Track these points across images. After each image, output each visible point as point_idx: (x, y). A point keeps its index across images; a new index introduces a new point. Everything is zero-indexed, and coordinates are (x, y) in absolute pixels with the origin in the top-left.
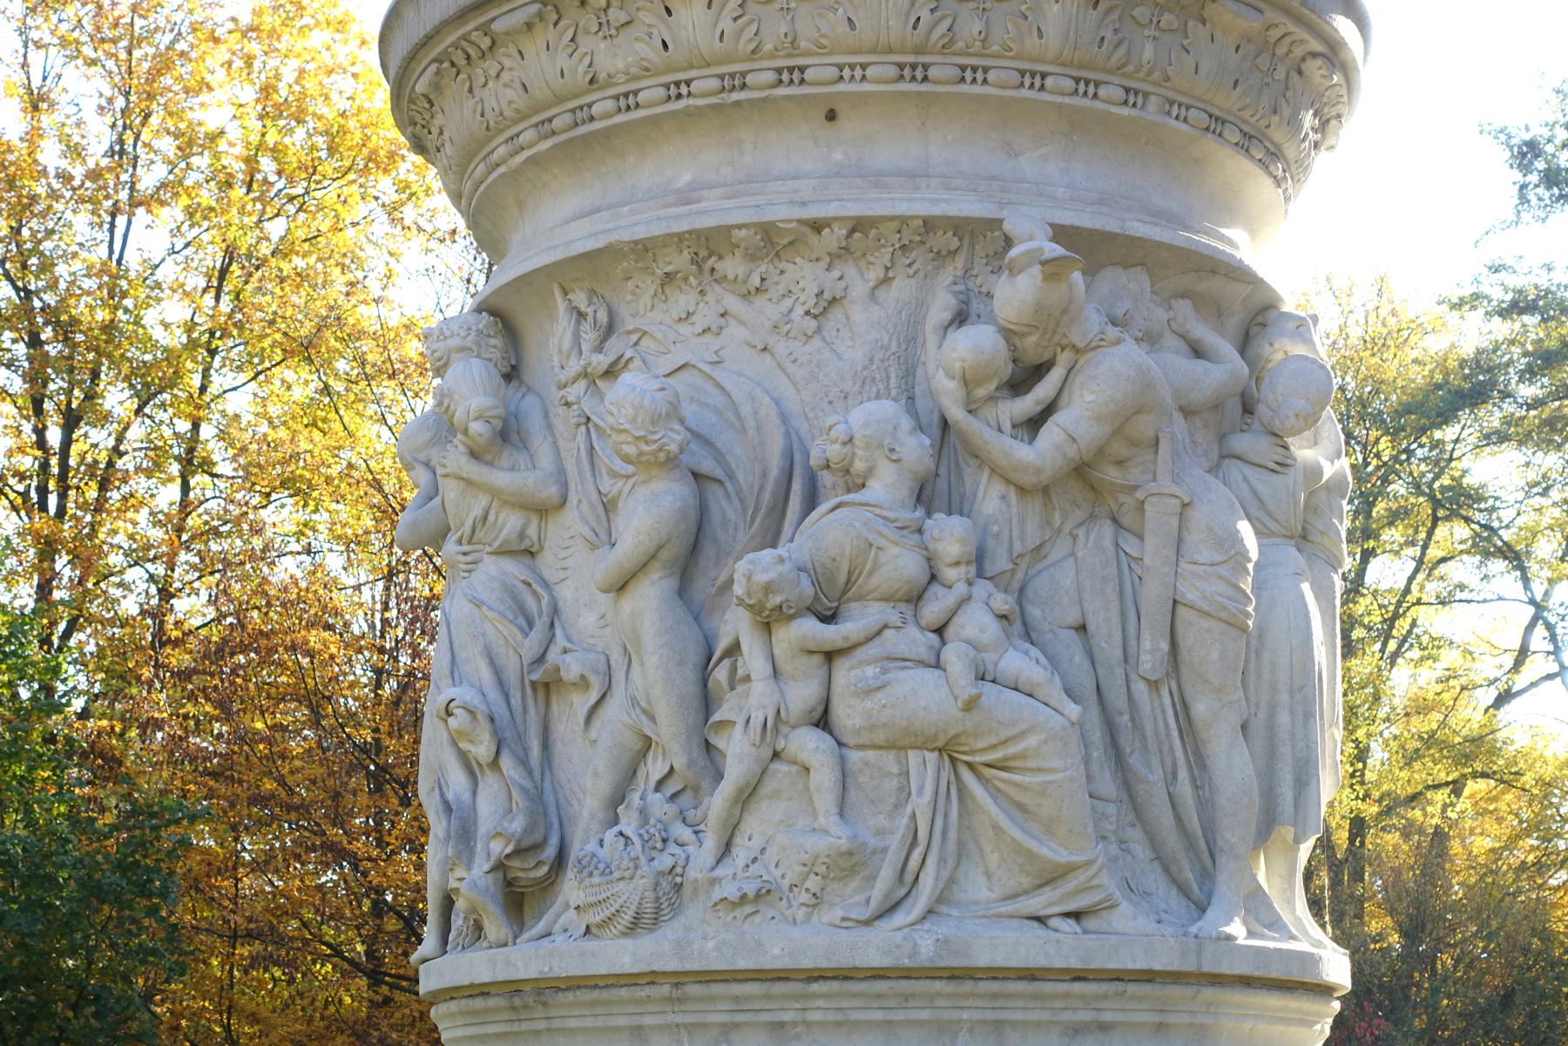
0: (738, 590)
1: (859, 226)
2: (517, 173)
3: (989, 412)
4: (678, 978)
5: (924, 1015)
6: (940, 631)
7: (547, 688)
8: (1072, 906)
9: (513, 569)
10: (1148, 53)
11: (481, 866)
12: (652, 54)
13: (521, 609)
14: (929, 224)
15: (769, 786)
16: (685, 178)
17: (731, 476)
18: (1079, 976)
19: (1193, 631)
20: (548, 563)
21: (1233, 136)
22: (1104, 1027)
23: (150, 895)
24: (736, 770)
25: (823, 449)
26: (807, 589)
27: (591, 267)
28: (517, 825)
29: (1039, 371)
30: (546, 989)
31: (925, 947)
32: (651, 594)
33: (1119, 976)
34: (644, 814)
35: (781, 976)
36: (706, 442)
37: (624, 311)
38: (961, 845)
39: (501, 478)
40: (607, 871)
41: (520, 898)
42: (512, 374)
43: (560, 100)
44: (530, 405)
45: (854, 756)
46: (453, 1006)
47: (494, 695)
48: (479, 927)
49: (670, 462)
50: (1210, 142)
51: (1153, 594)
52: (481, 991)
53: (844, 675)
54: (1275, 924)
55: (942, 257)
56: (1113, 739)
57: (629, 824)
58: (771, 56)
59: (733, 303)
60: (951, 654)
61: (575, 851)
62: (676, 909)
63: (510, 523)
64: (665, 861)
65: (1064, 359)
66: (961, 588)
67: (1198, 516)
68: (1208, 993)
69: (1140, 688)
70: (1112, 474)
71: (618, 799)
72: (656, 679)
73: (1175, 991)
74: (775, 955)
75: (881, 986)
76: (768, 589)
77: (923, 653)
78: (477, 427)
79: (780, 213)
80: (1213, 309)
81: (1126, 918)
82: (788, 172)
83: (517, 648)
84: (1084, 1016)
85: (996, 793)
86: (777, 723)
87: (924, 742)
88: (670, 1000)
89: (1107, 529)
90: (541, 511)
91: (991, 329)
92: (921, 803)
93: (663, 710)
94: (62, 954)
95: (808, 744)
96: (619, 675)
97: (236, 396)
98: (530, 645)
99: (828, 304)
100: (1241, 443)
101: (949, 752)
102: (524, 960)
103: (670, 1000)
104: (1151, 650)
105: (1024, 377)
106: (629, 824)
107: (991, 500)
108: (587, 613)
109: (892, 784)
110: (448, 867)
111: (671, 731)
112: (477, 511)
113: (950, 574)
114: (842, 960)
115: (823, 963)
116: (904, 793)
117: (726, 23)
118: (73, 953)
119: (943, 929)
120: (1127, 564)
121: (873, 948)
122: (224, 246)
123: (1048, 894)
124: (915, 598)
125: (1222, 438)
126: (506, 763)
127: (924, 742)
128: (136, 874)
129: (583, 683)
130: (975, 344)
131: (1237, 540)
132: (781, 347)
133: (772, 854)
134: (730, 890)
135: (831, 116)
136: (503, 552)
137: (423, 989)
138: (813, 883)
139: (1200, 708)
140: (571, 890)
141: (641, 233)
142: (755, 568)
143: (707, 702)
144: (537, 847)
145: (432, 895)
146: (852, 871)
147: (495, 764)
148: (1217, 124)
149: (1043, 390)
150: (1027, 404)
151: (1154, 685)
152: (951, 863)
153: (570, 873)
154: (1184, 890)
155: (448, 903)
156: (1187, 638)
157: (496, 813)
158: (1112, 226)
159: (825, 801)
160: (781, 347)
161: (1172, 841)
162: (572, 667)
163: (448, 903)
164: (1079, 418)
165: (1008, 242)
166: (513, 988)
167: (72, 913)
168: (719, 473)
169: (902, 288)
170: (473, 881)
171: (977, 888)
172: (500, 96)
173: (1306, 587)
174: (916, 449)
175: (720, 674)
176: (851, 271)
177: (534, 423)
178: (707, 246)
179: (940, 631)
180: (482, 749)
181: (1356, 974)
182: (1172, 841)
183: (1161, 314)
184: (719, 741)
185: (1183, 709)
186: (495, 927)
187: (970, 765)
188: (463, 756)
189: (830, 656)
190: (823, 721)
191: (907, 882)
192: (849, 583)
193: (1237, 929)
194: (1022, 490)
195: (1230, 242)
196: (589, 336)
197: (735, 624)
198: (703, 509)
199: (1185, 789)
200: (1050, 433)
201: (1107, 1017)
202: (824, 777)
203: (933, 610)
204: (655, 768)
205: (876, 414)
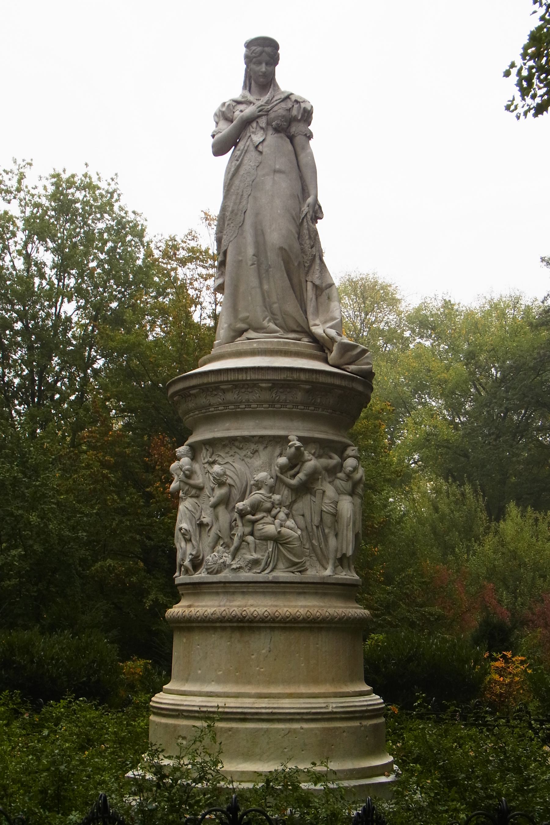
5: (270, 590)
8: (299, 570)
15: (242, 546)
17: (236, 485)
31: (270, 577)
46: (182, 587)
58: (244, 403)
59: (237, 450)
66: (278, 509)
84: (301, 590)
85: (286, 548)
86: (244, 535)
88: (223, 587)
95: (250, 539)
103: (223, 587)
114: (255, 580)
115: (251, 580)
119: (274, 574)
122: (270, 132)
123: (295, 567)
150: (292, 472)
152: (275, 561)
168: (234, 484)
187: (280, 544)
192: (257, 508)
201: (305, 591)
203: (274, 512)
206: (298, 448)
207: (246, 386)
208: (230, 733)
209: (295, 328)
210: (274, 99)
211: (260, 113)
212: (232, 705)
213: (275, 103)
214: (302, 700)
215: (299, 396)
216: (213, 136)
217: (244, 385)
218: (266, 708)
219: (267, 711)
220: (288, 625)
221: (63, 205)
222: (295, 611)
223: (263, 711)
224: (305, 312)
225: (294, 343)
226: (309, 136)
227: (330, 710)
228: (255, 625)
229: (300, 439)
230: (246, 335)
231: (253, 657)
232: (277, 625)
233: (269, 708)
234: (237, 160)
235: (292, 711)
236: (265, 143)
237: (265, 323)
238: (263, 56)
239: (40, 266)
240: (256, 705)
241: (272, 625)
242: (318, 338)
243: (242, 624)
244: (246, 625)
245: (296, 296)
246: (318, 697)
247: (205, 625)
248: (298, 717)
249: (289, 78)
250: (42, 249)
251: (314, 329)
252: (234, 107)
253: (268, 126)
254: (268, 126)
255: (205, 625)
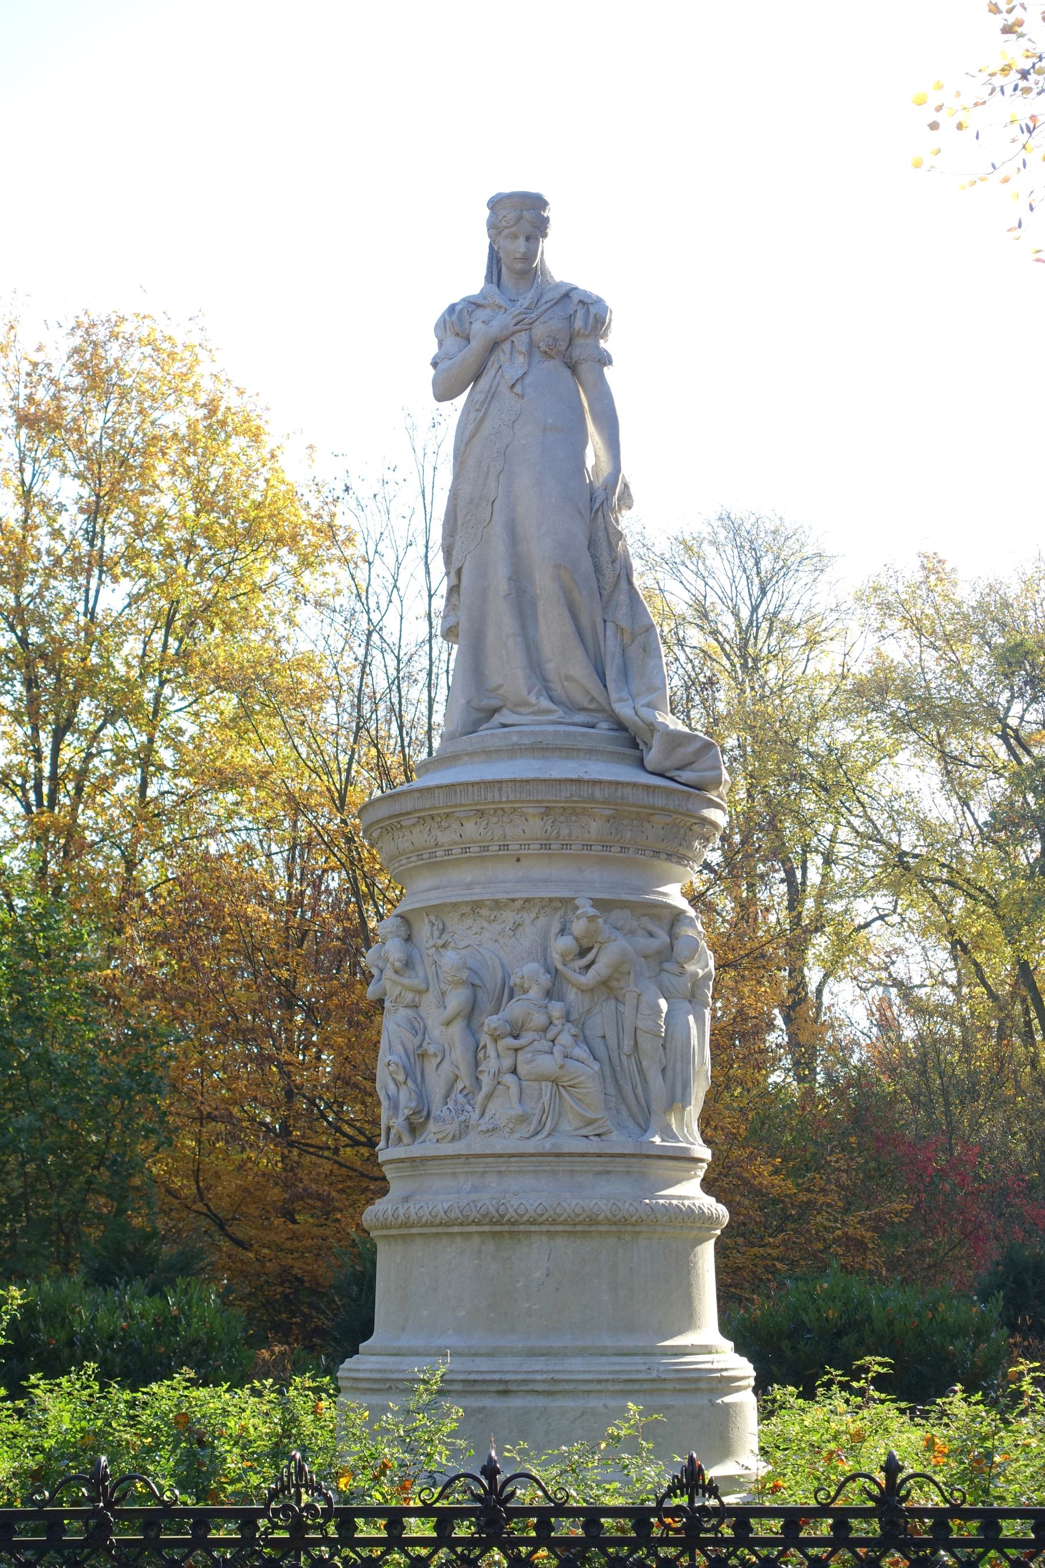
0: (485, 1029)
1: (527, 900)
2: (409, 869)
3: (571, 965)
4: (467, 1156)
6: (553, 1041)
7: (423, 1056)
9: (410, 1013)
10: (628, 835)
11: (401, 1118)
12: (457, 838)
13: (414, 1028)
14: (551, 900)
16: (469, 879)
18: (599, 1155)
19: (642, 1037)
20: (422, 1010)
21: (663, 856)
22: (608, 1172)
23: (150, 1092)
24: (485, 1088)
25: (515, 980)
26: (508, 1028)
27: (437, 909)
28: (413, 1104)
29: (590, 949)
30: (424, 1160)
31: (548, 1146)
32: (458, 1027)
33: (613, 1155)
34: (456, 1102)
35: (501, 1156)
36: (476, 973)
37: (448, 924)
38: (560, 1113)
39: (406, 981)
40: (444, 1121)
41: (414, 1129)
42: (409, 939)
43: (425, 849)
44: (415, 952)
45: (524, 1083)
47: (405, 1058)
48: (400, 1139)
49: (463, 983)
50: (655, 861)
51: (628, 1025)
52: (402, 1161)
53: (521, 1056)
54: (675, 1138)
55: (556, 909)
56: (612, 1074)
57: (451, 1105)
59: (485, 924)
60: (555, 1049)
61: (433, 1114)
62: (467, 1133)
63: (409, 996)
64: (462, 1118)
65: (597, 946)
67: (644, 998)
68: (645, 1161)
69: (624, 1057)
70: (615, 984)
71: (447, 1096)
72: (459, 1055)
73: (633, 1160)
74: (499, 1149)
75: (533, 1159)
76: (495, 1029)
77: (547, 1049)
78: (397, 964)
79: (500, 896)
80: (657, 918)
81: (615, 1136)
82: (503, 879)
83: (413, 1042)
87: (547, 1079)
89: (613, 1002)
90: (420, 992)
91: (570, 938)
92: (546, 1099)
93: (461, 1067)
94: (89, 1132)
95: (509, 1079)
96: (447, 1052)
97: (179, 714)
98: (417, 1041)
99: (517, 926)
100: (667, 966)
101: (555, 1082)
102: (416, 1150)
104: (627, 1044)
105: (583, 952)
106: (451, 1105)
107: (572, 994)
108: (436, 1031)
109: (536, 1093)
110: (389, 1119)
111: (464, 1072)
112: (397, 992)
113: (556, 1022)
114: (521, 1151)
116: (540, 1096)
117: (481, 830)
118: (98, 1132)
120: (619, 1016)
121: (530, 1147)
123: (589, 1128)
124: (545, 1030)
125: (661, 963)
126: (409, 1082)
127: (547, 1079)
128: (140, 1075)
129: (435, 1055)
130: (563, 944)
131: (658, 1006)
132: (501, 941)
133: (497, 1116)
134: (483, 1128)
135: (518, 860)
136: (406, 1007)
137: (380, 1160)
138: (511, 1125)
139: (645, 1064)
140: (432, 1127)
141: (454, 900)
142: (491, 1022)
143: (477, 1064)
144: (420, 1112)
145: (383, 1127)
146: (523, 1121)
147: (405, 1083)
148: (657, 853)
149: (590, 957)
151: (629, 1056)
153: (431, 1121)
154: (639, 1126)
155: (389, 1129)
156: (640, 1040)
157: (406, 1100)
158: (616, 897)
159: (515, 1099)
160: (501, 941)
161: (635, 1109)
162: (431, 1049)
163: (389, 1129)
164: (604, 963)
165: (577, 908)
166: (413, 1160)
167: (98, 1105)
169: (542, 920)
170: (398, 1123)
171: (566, 1126)
172: (404, 844)
173: (691, 1018)
174: (545, 980)
175: (481, 1055)
176: (525, 914)
177: (417, 959)
178: (476, 906)
179: (553, 1041)
180: (401, 1078)
181: (713, 1155)
182: (635, 1109)
183: (635, 924)
184: (480, 1077)
185: (639, 1064)
186: (406, 1139)
188: (394, 1079)
189: (516, 1050)
190: (514, 1071)
191: (541, 1124)
193: (657, 1140)
194: (582, 991)
195: (665, 894)
196: (436, 933)
197: (485, 1039)
198: (475, 997)
199: (639, 1090)
200: (592, 971)
202: (514, 1090)
203: (550, 1035)
204: (460, 1086)
205: (532, 967)
206: (592, 919)
207: (500, 813)
208: (481, 1416)
209: (586, 704)
210: (543, 301)
211: (518, 327)
212: (484, 1368)
213: (544, 308)
214: (604, 1359)
215: (595, 827)
216: (435, 364)
217: (495, 810)
218: (542, 1372)
219: (545, 1376)
220: (579, 1228)
221: (96, 377)
222: (592, 1204)
223: (538, 1377)
224: (602, 677)
225: (583, 734)
226: (605, 360)
227: (654, 1375)
228: (522, 1228)
229: (597, 903)
230: (498, 719)
231: (519, 1285)
232: (560, 1228)
233: (547, 1372)
234: (478, 410)
235: (588, 1377)
236: (528, 380)
237: (533, 699)
238: (519, 219)
239: (52, 508)
240: (525, 1368)
241: (552, 1228)
242: (627, 724)
243: (498, 1228)
244: (506, 1228)
245: (586, 649)
246: (633, 1355)
247: (434, 1230)
248: (598, 1387)
249: (563, 259)
250: (55, 474)
251: (617, 707)
252: (470, 314)
253: (527, 346)
254: (527, 346)
255: (434, 1230)
